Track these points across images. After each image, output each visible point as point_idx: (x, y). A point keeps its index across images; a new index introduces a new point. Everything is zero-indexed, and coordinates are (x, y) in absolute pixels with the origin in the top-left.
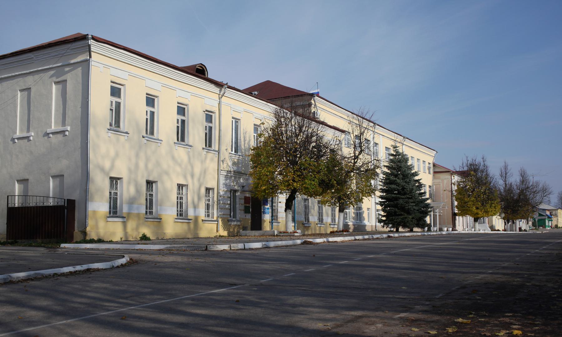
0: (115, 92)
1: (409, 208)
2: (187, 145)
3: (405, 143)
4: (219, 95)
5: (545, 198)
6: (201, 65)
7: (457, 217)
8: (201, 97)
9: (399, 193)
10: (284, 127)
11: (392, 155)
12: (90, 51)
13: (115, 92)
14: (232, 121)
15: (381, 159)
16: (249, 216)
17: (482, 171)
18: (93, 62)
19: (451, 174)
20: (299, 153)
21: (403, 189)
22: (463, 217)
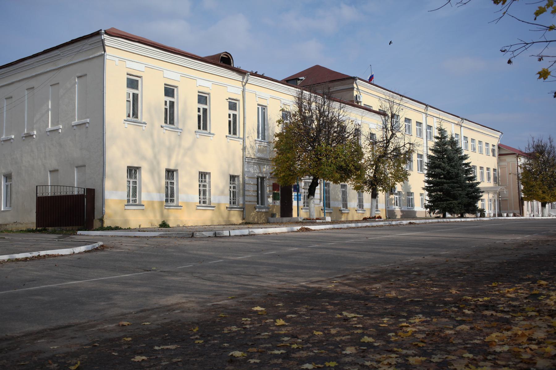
0: (133, 83)
1: (454, 193)
3: (463, 125)
4: (242, 82)
6: (226, 54)
7: (525, 202)
8: (223, 85)
9: (445, 178)
10: (307, 113)
11: (437, 138)
12: (104, 46)
13: (133, 83)
14: (258, 108)
15: (415, 142)
16: (278, 203)
18: (107, 56)
19: (517, 156)
20: (348, 137)
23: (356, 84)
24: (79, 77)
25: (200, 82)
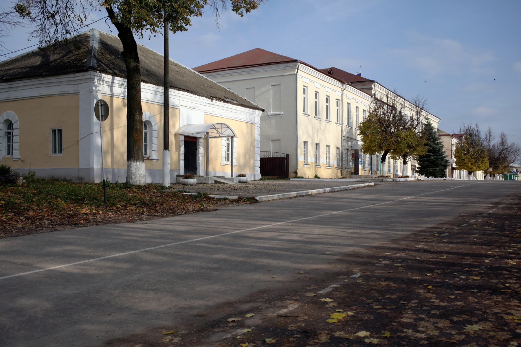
2: (329, 121)
5: (517, 157)
7: (454, 171)
17: (476, 135)
21: (434, 148)
22: (460, 171)
23: (374, 85)
24: (272, 86)
25: (327, 89)
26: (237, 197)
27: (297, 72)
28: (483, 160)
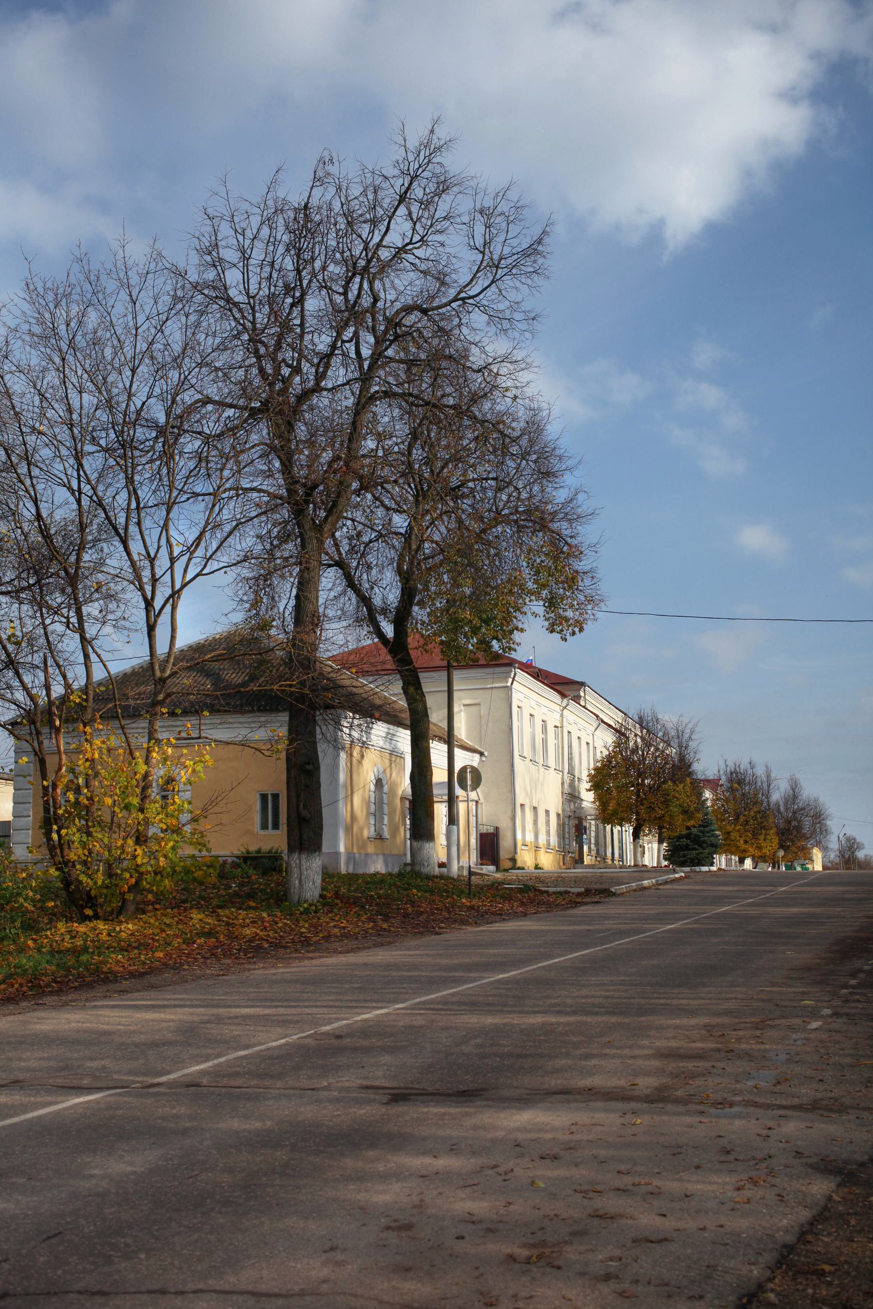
24: (464, 705)
26: (583, 890)
27: (512, 684)
28: (766, 835)
